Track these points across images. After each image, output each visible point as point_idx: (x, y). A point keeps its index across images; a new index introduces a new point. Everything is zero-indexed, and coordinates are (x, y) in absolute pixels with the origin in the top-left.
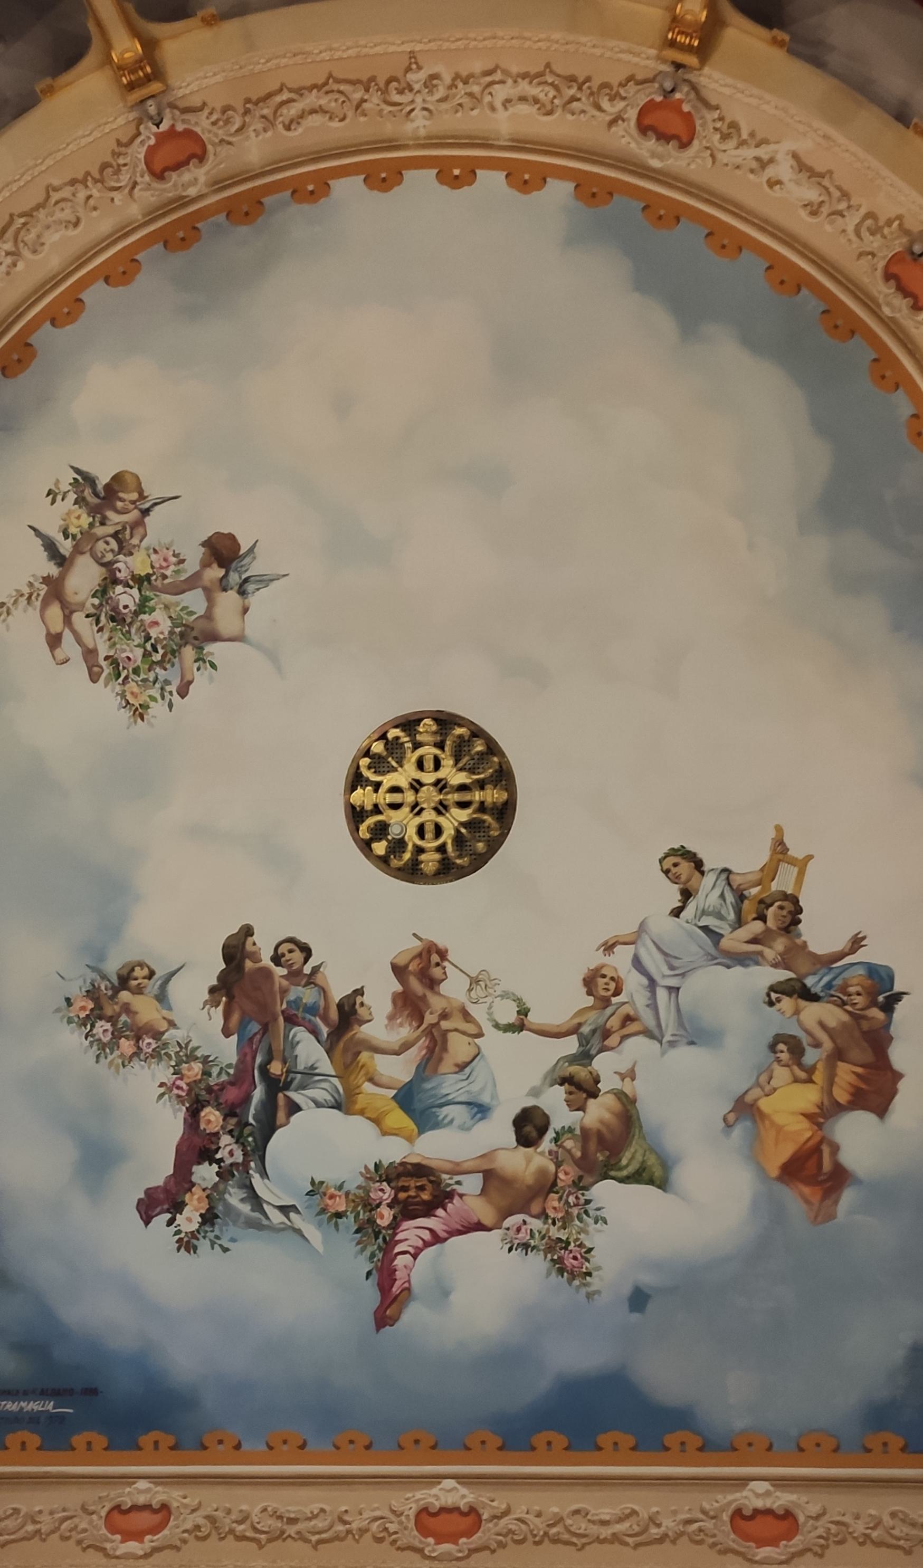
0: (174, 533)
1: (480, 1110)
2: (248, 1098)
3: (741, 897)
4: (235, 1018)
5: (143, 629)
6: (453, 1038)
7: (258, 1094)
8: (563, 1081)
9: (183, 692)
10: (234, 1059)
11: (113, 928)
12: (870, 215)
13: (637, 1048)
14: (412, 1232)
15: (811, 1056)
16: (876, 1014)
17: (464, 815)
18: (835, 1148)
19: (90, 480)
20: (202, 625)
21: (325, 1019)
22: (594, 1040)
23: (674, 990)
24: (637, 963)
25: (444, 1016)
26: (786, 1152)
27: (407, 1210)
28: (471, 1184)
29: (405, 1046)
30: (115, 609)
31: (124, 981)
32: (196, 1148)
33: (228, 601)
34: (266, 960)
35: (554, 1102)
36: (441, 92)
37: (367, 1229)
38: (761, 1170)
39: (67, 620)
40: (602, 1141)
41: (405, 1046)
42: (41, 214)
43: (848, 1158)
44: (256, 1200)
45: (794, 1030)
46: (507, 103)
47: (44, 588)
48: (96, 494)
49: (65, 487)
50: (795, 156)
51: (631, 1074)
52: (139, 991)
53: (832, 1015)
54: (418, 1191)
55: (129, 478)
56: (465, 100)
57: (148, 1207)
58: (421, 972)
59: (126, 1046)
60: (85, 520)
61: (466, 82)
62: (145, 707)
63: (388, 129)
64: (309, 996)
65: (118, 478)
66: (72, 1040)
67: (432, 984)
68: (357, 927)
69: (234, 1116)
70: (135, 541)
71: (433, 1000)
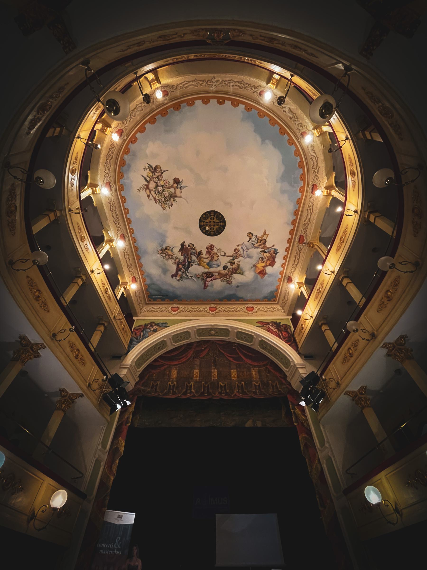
0: (168, 177)
1: (218, 266)
2: (185, 264)
3: (258, 239)
4: (183, 254)
5: (164, 195)
6: (215, 257)
7: (187, 263)
8: (230, 262)
9: (172, 205)
10: (183, 259)
11: (164, 241)
12: (301, 123)
13: (241, 258)
14: (208, 279)
15: (264, 260)
16: (275, 255)
17: (217, 227)
18: (265, 270)
19: (151, 166)
20: (174, 194)
21: (196, 254)
22: (235, 257)
23: (247, 251)
24: (242, 248)
25: (214, 254)
26: (259, 271)
27: (208, 277)
28: (217, 274)
29: (208, 258)
30: (158, 191)
31: (166, 249)
32: (178, 270)
33: (178, 190)
34: (187, 246)
35: (229, 265)
36: (219, 83)
37: (202, 279)
38: (255, 273)
39: (150, 193)
40: (235, 269)
41: (208, 258)
42: (135, 110)
43: (267, 272)
44: (187, 276)
45: (262, 256)
46: (233, 86)
47: (145, 187)
48: (152, 169)
49: (147, 167)
50: (290, 108)
51: (240, 262)
52: (168, 250)
53: (268, 255)
54: (210, 275)
55: (159, 167)
56: (224, 85)
57: (172, 276)
58: (210, 249)
59: (167, 257)
60: (151, 174)
61: (225, 81)
62: (165, 208)
63: (207, 88)
64: (194, 251)
65: (156, 166)
66: (159, 256)
67: (212, 250)
68: (201, 242)
69: (183, 266)
70: (161, 179)
71: (213, 252)
